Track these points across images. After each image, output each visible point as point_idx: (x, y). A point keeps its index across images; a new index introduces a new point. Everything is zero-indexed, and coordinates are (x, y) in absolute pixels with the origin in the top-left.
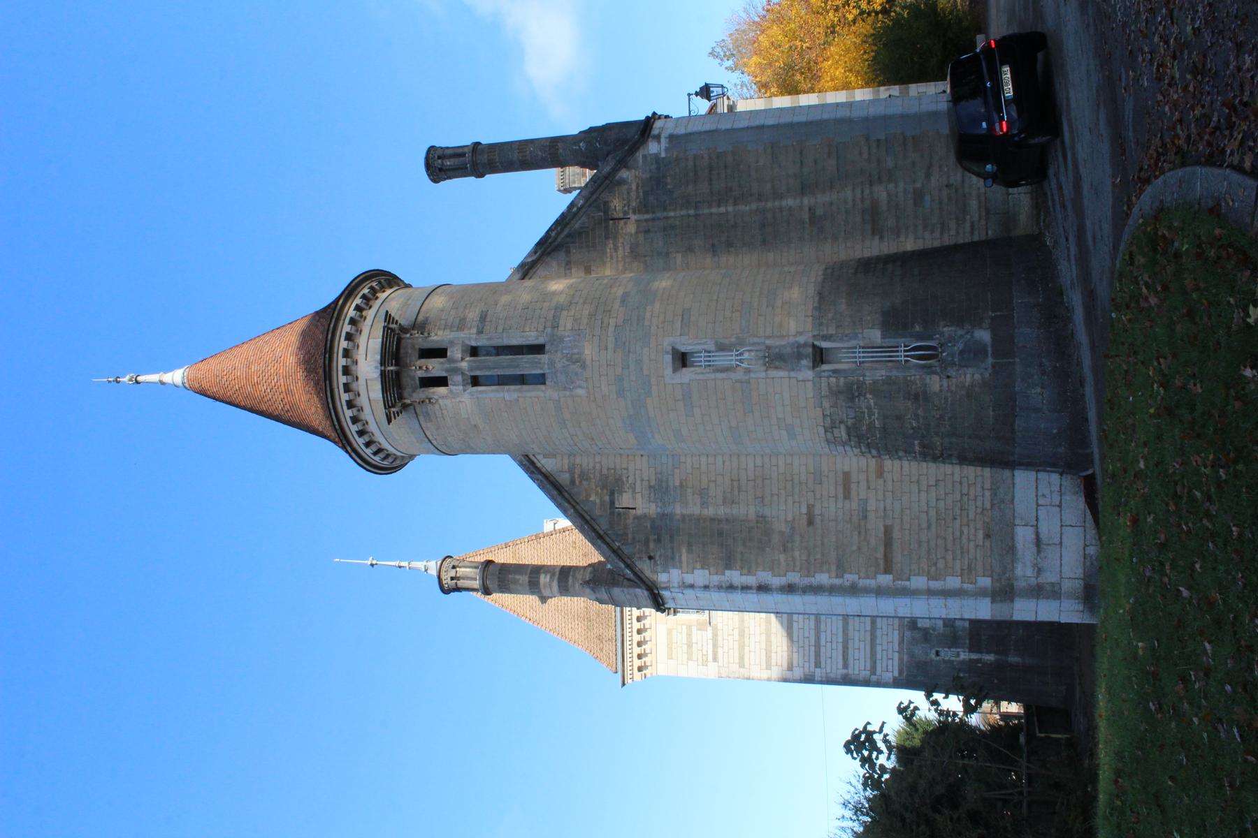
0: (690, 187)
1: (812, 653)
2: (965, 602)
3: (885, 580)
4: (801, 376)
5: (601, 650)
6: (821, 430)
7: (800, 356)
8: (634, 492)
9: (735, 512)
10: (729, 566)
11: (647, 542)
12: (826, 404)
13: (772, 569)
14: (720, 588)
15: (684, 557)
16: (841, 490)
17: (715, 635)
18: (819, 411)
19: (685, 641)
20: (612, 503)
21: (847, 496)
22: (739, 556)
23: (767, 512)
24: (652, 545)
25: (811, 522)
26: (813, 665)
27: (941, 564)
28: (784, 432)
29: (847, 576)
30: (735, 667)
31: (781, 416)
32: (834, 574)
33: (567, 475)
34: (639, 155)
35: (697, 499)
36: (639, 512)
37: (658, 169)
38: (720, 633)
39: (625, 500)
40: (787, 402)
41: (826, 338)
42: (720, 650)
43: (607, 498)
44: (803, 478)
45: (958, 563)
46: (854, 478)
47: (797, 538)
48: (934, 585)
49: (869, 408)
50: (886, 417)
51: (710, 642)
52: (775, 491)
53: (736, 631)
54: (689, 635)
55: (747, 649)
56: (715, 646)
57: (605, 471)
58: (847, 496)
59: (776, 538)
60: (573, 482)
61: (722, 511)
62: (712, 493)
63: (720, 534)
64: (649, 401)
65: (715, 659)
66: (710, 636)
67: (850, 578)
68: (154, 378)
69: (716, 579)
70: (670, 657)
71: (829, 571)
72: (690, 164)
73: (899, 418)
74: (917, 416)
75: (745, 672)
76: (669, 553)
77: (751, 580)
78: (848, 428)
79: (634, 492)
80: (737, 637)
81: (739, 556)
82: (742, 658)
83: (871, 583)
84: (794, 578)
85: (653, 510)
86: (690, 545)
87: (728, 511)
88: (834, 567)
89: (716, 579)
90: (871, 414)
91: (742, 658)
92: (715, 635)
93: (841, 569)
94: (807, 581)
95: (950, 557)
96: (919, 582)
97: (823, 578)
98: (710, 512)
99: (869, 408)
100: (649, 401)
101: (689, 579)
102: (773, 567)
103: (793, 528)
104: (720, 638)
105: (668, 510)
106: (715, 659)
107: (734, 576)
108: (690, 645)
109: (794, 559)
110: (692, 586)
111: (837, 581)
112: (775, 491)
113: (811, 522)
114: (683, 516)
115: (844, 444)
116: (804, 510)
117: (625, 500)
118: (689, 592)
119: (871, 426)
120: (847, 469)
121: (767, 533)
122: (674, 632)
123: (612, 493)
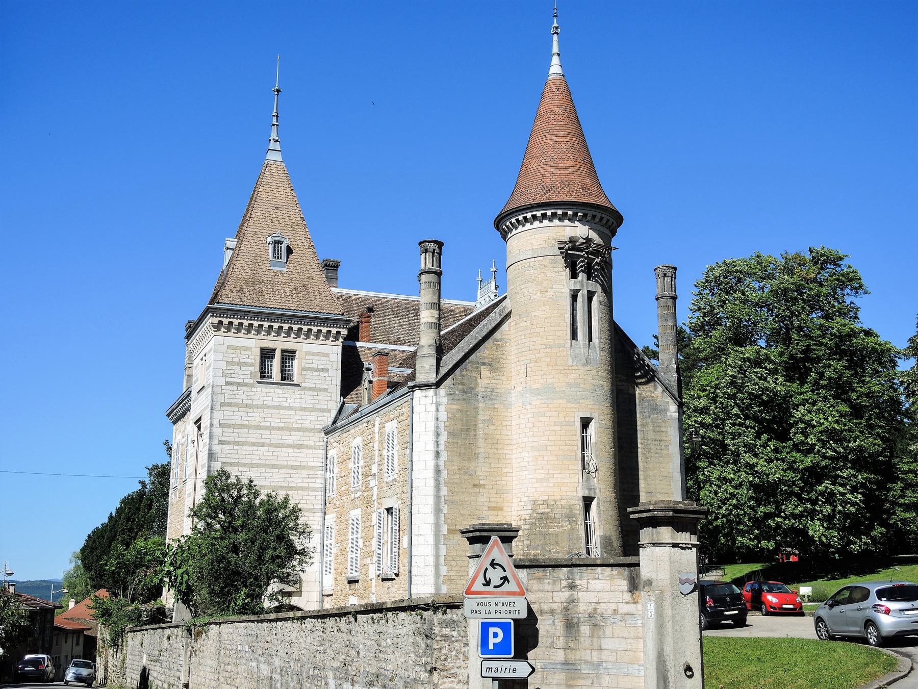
0: (651, 428)
1: (233, 461)
2: (432, 577)
3: (444, 530)
4: (580, 489)
5: (231, 291)
6: (546, 498)
7: (590, 489)
8: (490, 379)
9: (480, 440)
10: (450, 434)
11: (463, 384)
12: (563, 502)
13: (449, 461)
14: (437, 427)
15: (455, 407)
16: (494, 505)
17: (246, 385)
18: (558, 498)
19: (242, 360)
20: (484, 364)
21: (490, 508)
22: (456, 441)
23: (481, 460)
24: (461, 387)
25: (475, 486)
26: (224, 460)
27: (453, 563)
28: (543, 476)
29: (446, 506)
30: (221, 398)
31: (555, 476)
32: (447, 498)
33: (499, 337)
34: (669, 399)
35: (487, 418)
36: (479, 380)
37: (661, 410)
38: (249, 389)
39: (485, 371)
40: (564, 480)
41: (598, 504)
42: (235, 388)
43: (486, 361)
44: (499, 483)
45: (454, 573)
46: (499, 513)
47: (466, 477)
48: (442, 559)
49: (562, 526)
50: (557, 535)
51: (240, 381)
52: (492, 465)
53: (249, 402)
54: (246, 364)
55: (236, 409)
56: (238, 384)
57: (502, 361)
58: (490, 508)
59: (467, 464)
60: (495, 340)
61: (480, 433)
62: (491, 427)
63: (467, 430)
64: (565, 401)
65: (227, 383)
66: (246, 381)
67: (445, 508)
68: (555, 49)
69: (442, 425)
70: (229, 347)
71: (448, 495)
72: (663, 429)
73: (557, 543)
74: (559, 552)
75: (217, 406)
76: (456, 397)
77: (442, 448)
78: (548, 513)
79: (490, 379)
80: (245, 402)
81: (456, 441)
82: (229, 405)
83: (442, 522)
84: (444, 474)
85: (481, 389)
86: (462, 411)
87: (481, 436)
88: (450, 498)
89: (442, 425)
90: (559, 527)
91: (229, 405)
92: (246, 385)
93: (449, 503)
94: (442, 481)
95: (458, 568)
96: (443, 550)
97: (444, 492)
98: (480, 425)
99: (562, 526)
100: (565, 401)
101: (442, 408)
102: (449, 461)
103: (472, 475)
104: (244, 389)
105: (480, 399)
106: (227, 383)
107: (444, 437)
108: (239, 364)
109: (454, 474)
110: (437, 410)
111: (442, 501)
112: (492, 465)
113: (475, 486)
114: (477, 408)
115: (534, 510)
116: (482, 482)
117: (485, 371)
118: (434, 408)
119: (550, 527)
120: (505, 509)
121: (469, 459)
122: (248, 353)
123: (490, 365)
